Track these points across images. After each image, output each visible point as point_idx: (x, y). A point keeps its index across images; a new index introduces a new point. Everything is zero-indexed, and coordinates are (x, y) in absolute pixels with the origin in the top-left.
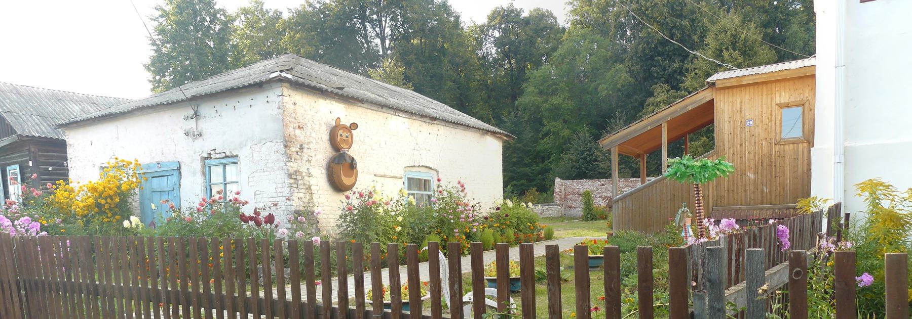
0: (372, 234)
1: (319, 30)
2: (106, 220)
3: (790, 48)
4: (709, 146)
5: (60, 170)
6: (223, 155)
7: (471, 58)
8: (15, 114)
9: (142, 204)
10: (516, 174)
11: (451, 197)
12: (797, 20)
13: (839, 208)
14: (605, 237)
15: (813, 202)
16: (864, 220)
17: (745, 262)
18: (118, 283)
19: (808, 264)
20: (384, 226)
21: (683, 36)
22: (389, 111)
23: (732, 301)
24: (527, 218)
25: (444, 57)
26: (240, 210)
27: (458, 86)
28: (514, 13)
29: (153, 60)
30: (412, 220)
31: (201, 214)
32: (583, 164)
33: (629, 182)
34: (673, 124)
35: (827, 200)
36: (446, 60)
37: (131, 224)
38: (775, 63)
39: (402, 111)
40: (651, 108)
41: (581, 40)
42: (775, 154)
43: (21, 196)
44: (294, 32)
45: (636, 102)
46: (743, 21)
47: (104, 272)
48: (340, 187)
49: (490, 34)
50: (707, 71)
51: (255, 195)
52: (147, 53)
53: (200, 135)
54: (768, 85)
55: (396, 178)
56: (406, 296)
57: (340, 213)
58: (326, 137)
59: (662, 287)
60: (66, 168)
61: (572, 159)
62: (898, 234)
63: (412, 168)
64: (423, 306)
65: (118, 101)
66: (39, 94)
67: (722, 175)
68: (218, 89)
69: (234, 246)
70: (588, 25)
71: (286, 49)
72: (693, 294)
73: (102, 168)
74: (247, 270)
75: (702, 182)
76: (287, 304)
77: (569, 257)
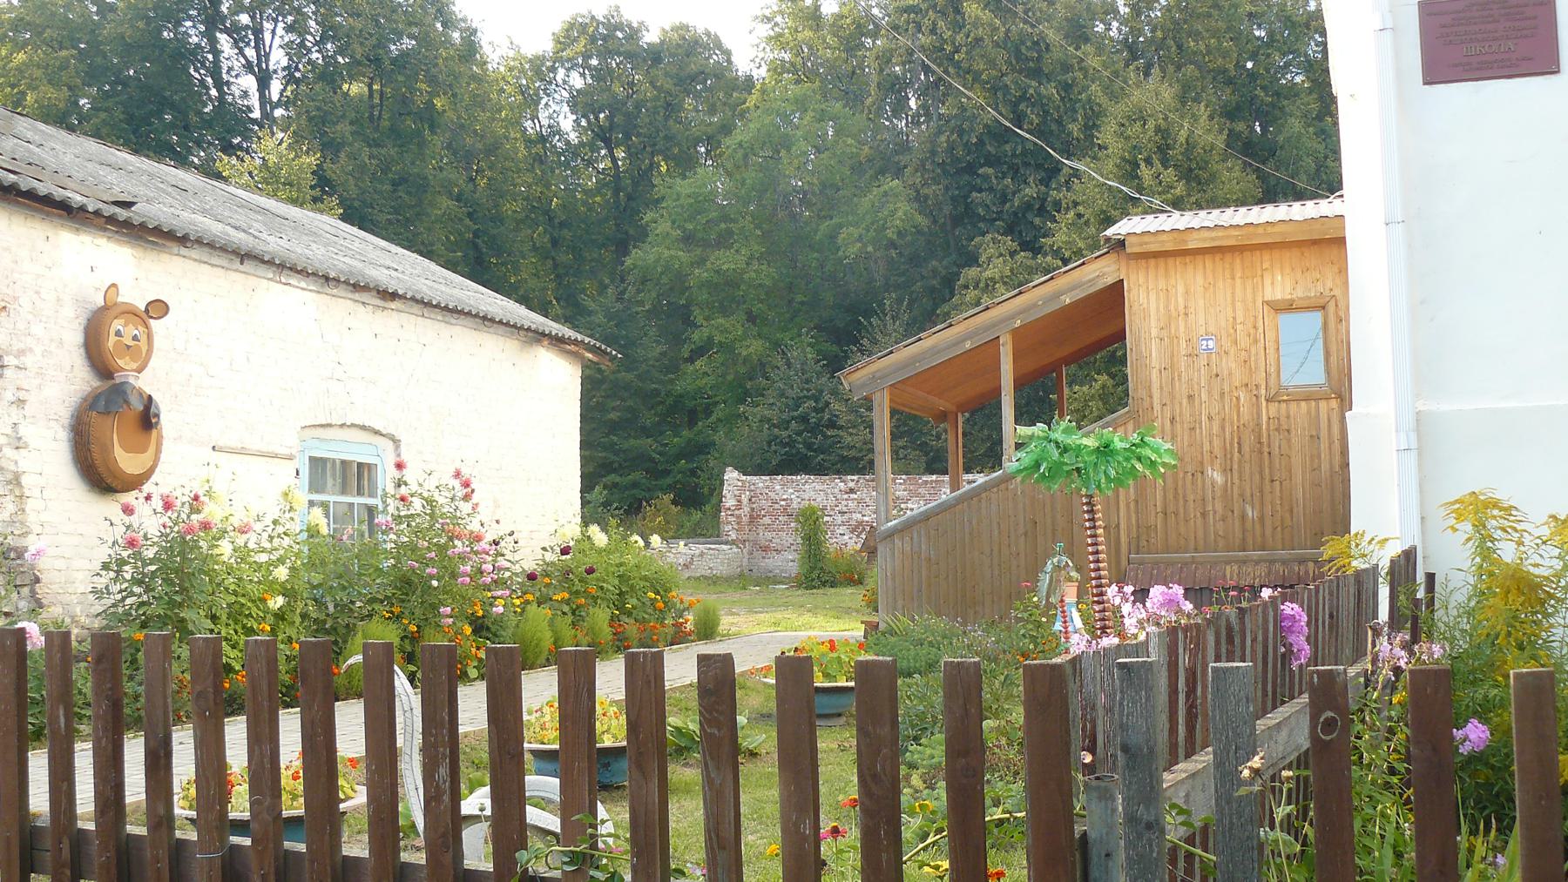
0: (196, 618)
1: (82, 46)
3: (1287, 170)
4: (1116, 398)
7: (507, 138)
10: (616, 453)
11: (432, 515)
12: (1298, 107)
13: (1412, 557)
14: (859, 631)
15: (1357, 545)
16: (1464, 591)
17: (1210, 696)
19: (1350, 700)
20: (235, 593)
21: (1044, 122)
23: (1180, 802)
24: (645, 578)
25: (433, 132)
30: (317, 578)
33: (920, 485)
38: (1257, 204)
39: (299, 272)
40: (971, 294)
41: (793, 112)
42: (1268, 424)
44: (9, 46)
45: (934, 277)
46: (1182, 99)
50: (1104, 212)
54: (1245, 253)
55: (276, 456)
56: (294, 797)
57: (104, 553)
58: (74, 337)
59: (1008, 767)
61: (769, 420)
62: (1534, 622)
64: (345, 828)
70: (811, 74)
72: (1086, 784)
75: (1100, 491)
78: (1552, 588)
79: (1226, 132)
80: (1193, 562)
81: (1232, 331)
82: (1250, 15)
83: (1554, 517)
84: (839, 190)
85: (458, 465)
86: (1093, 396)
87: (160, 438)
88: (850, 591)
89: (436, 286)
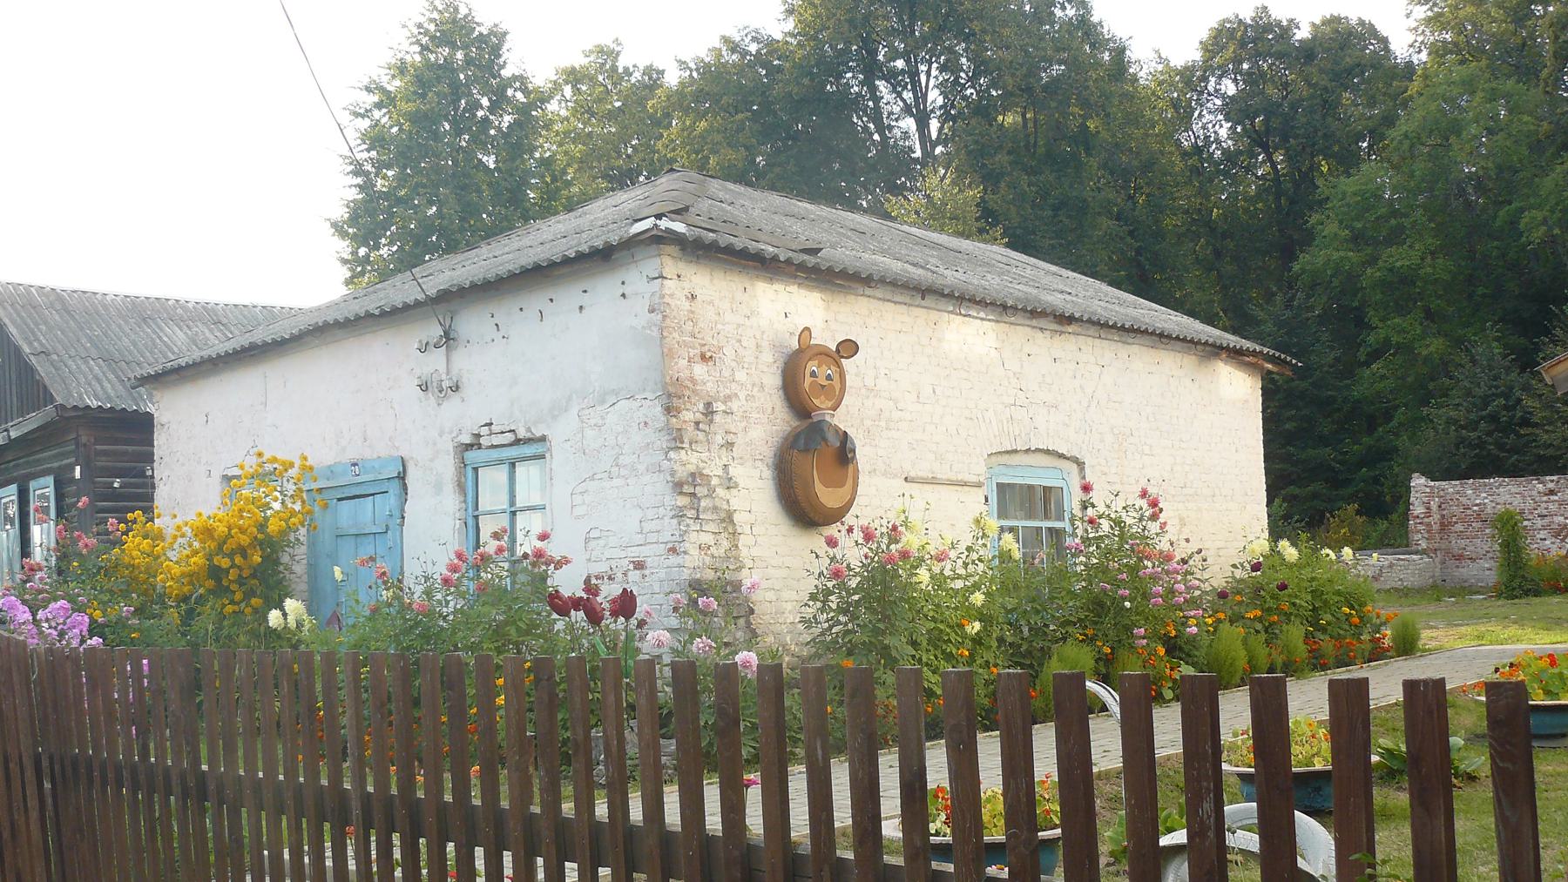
0: (898, 643)
1: (755, 108)
2: (229, 609)
5: (137, 486)
6: (509, 437)
8: (55, 357)
9: (312, 567)
11: (1121, 536)
18: (251, 768)
20: (934, 619)
22: (943, 303)
24: (1338, 593)
25: (1089, 154)
26: (549, 582)
27: (1131, 228)
28: (1272, 31)
29: (355, 210)
30: (1011, 602)
31: (452, 593)
32: (1489, 434)
36: (1094, 163)
37: (286, 619)
43: (55, 550)
47: (221, 742)
48: (812, 515)
49: (1211, 88)
51: (587, 540)
52: (340, 194)
53: (456, 388)
55: (965, 484)
57: (810, 585)
58: (773, 380)
60: (149, 480)
63: (1007, 456)
65: (270, 314)
66: (105, 307)
68: (502, 270)
69: (532, 677)
70: (1477, 53)
71: (672, 161)
73: (227, 479)
74: (565, 742)
76: (666, 837)
77: (1472, 706)
84: (1517, 172)
85: (1143, 483)
87: (857, 471)
89: (1110, 306)
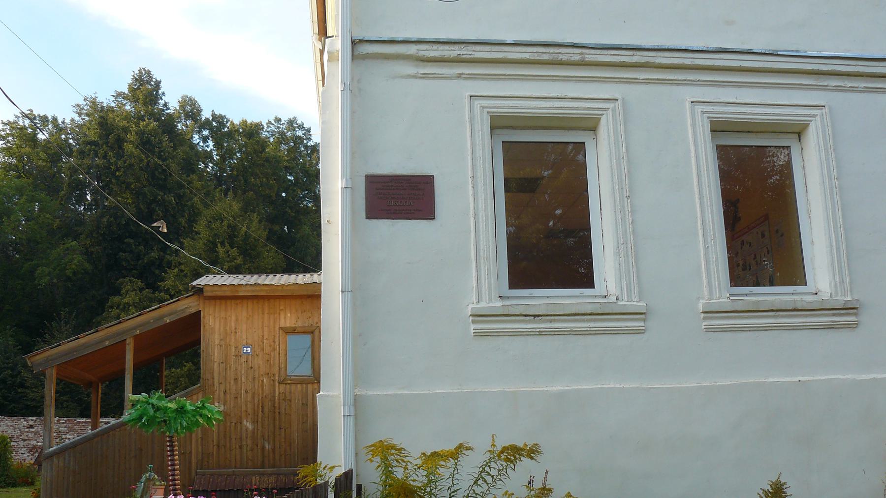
12: (309, 220)
34: (143, 341)
35: (334, 467)
40: (115, 312)
41: (14, 195)
42: (279, 396)
67: (205, 424)
70: (28, 174)
75: (177, 433)
78: (422, 493)
79: (267, 230)
80: (233, 475)
81: (261, 343)
82: (286, 167)
83: (424, 454)
86: (183, 375)
88: (24, 490)
